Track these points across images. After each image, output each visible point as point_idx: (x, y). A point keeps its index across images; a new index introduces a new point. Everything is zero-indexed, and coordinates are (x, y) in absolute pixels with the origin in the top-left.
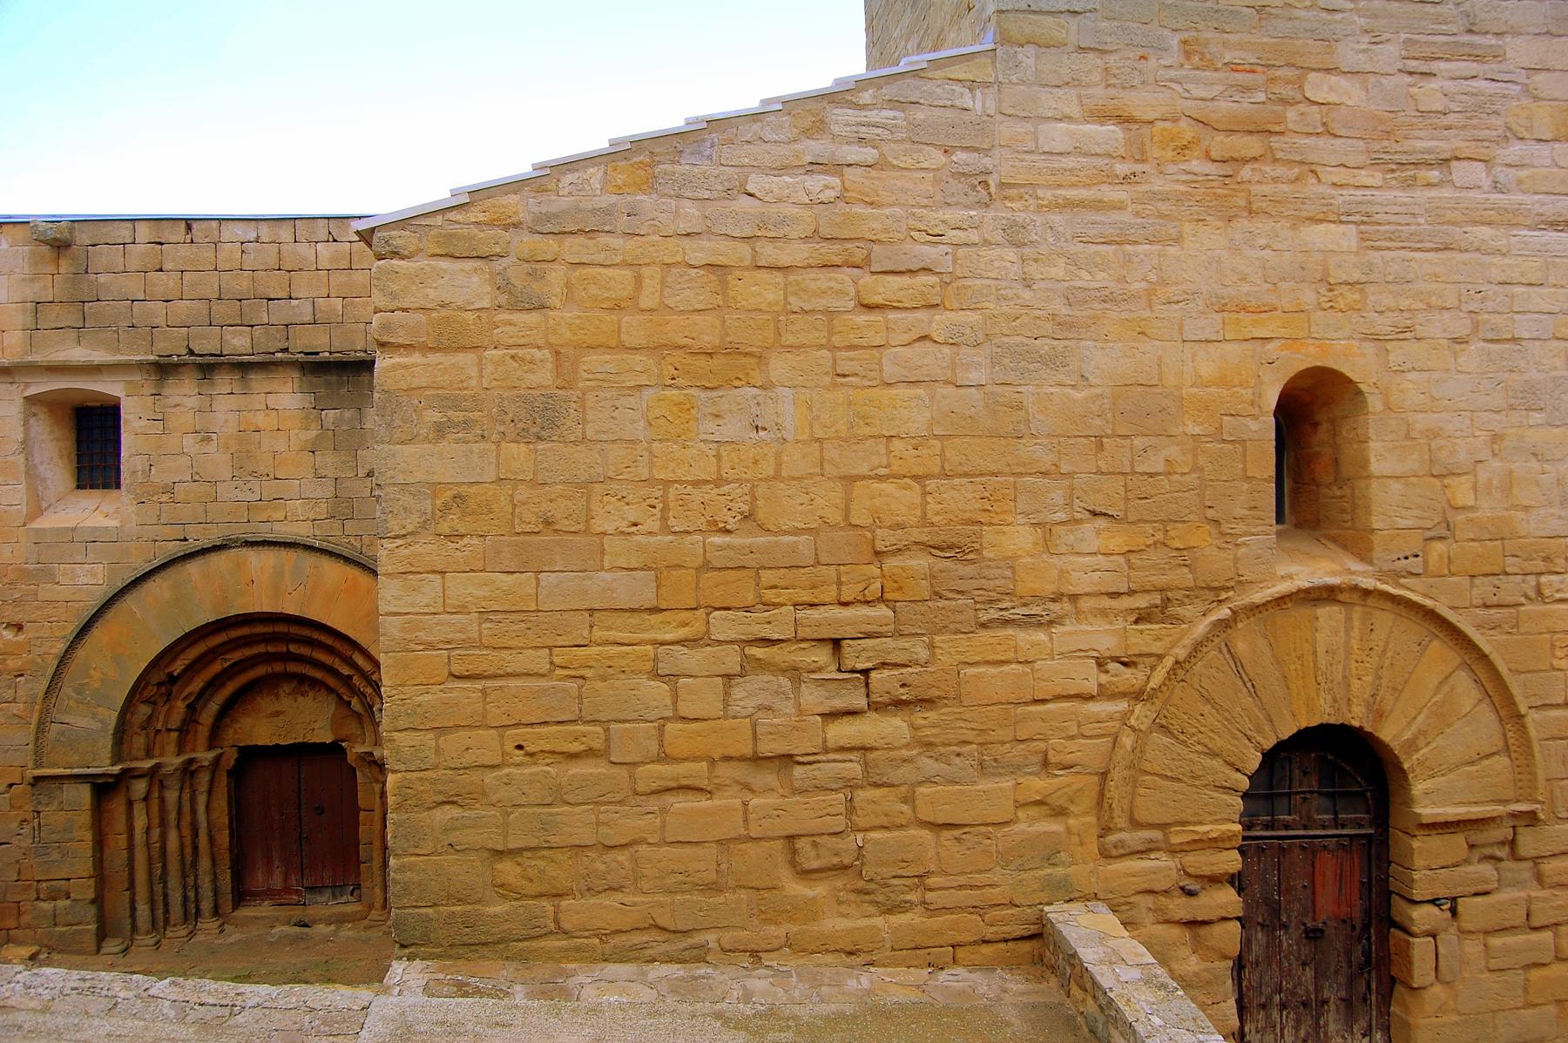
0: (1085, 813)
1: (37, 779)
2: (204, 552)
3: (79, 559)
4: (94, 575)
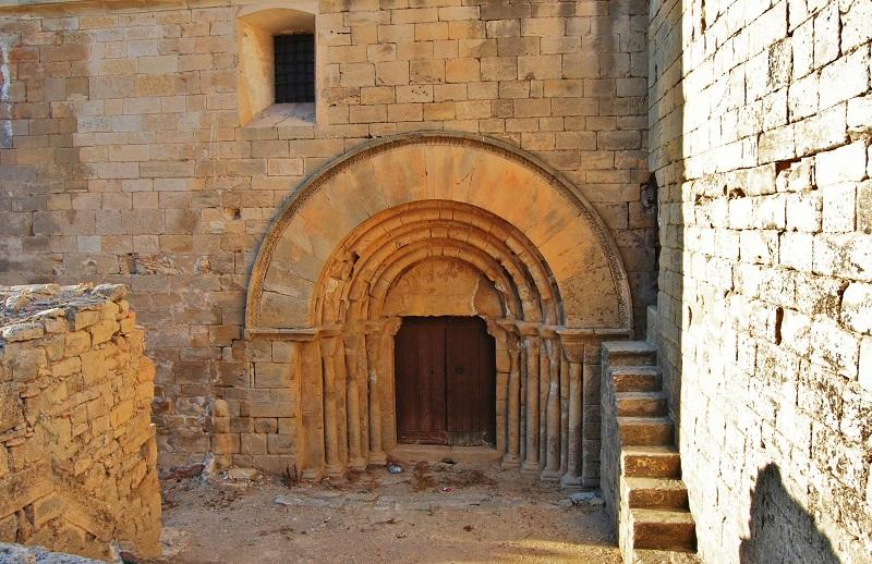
2: (386, 147)
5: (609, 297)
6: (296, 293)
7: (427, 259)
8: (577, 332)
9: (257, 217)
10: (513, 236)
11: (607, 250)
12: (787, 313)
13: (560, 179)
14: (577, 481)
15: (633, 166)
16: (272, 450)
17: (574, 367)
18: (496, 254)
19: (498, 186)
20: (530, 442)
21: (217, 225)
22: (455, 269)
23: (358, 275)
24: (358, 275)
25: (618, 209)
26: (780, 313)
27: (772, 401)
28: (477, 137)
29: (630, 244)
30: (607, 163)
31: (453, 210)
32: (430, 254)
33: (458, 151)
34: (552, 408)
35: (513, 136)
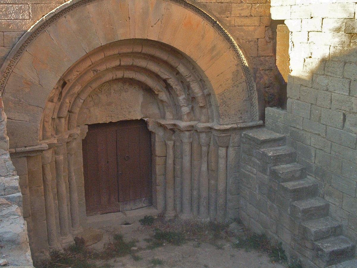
12: (348, 115)
25: (252, 43)
26: (344, 115)
27: (86, 125)
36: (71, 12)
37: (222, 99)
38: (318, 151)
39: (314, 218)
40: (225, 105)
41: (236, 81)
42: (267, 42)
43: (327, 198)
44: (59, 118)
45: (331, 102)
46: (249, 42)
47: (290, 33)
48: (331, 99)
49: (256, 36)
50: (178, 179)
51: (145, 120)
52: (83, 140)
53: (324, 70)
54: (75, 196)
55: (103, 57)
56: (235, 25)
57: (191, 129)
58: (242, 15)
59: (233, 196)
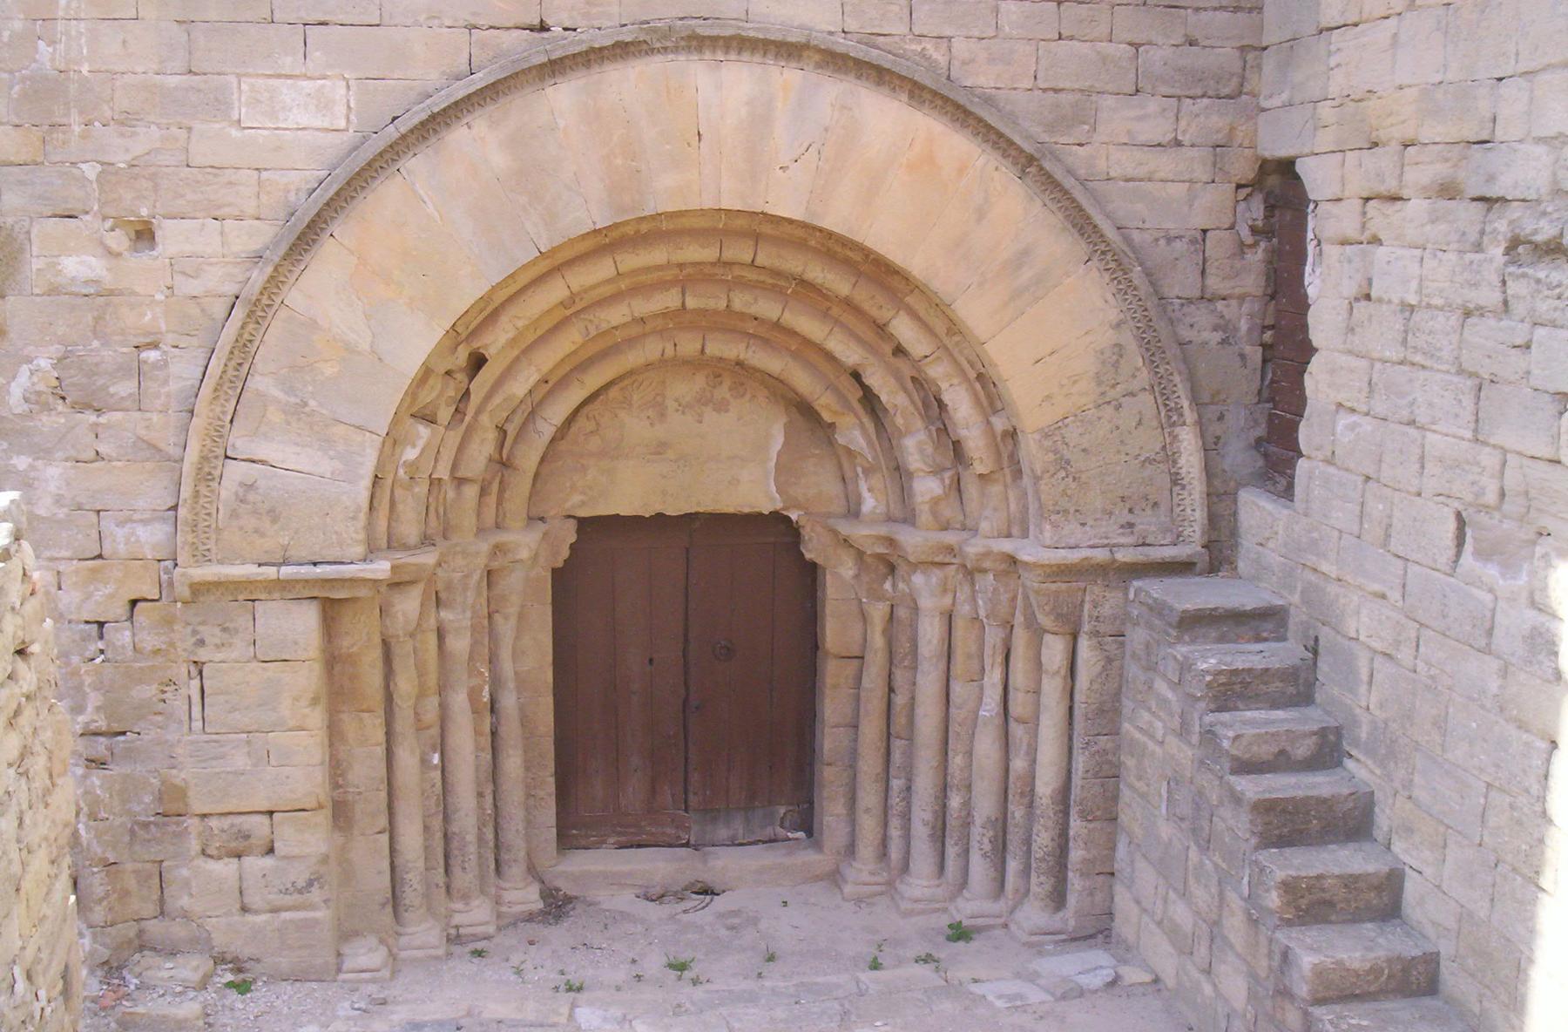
0: (104, 945)
1: (199, 590)
2: (591, 57)
3: (288, 63)
4: (325, 106)
5: (1149, 470)
6: (326, 466)
7: (663, 363)
8: (1074, 557)
9: (210, 252)
10: (914, 315)
11: (1152, 351)
13: (1047, 165)
14: (1056, 921)
15: (1219, 138)
16: (254, 900)
17: (1054, 651)
18: (850, 354)
19: (885, 176)
20: (920, 832)
21: (80, 266)
22: (723, 392)
23: (478, 412)
24: (478, 412)
28: (841, 44)
29: (1206, 335)
30: (1159, 130)
31: (757, 238)
32: (670, 352)
33: (788, 78)
34: (986, 747)
35: (929, 46)
36: (491, 108)
37: (1056, 452)
38: (1379, 660)
39: (1333, 918)
40: (1063, 474)
41: (1113, 386)
42: (1242, 244)
43: (1398, 847)
44: (460, 482)
45: (1423, 467)
46: (1170, 240)
47: (1312, 206)
48: (1422, 457)
49: (1200, 221)
50: (898, 746)
51: (789, 518)
52: (557, 574)
53: (1404, 342)
54: (513, 763)
55: (722, 304)
56: (1112, 174)
57: (947, 560)
58: (1142, 138)
59: (1091, 826)
